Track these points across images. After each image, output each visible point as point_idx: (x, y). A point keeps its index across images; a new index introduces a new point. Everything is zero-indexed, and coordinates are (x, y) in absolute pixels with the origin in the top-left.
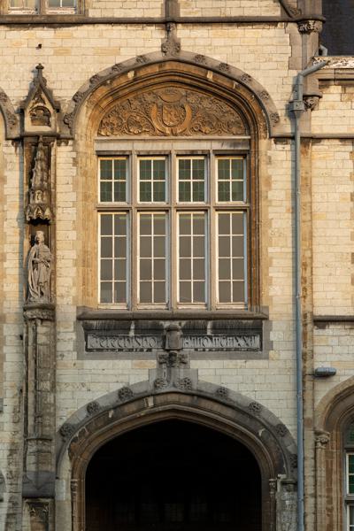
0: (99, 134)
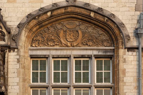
0: (31, 46)
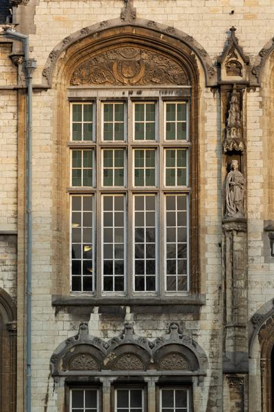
0: (72, 84)
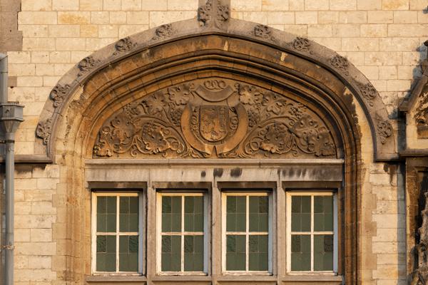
0: (96, 154)
